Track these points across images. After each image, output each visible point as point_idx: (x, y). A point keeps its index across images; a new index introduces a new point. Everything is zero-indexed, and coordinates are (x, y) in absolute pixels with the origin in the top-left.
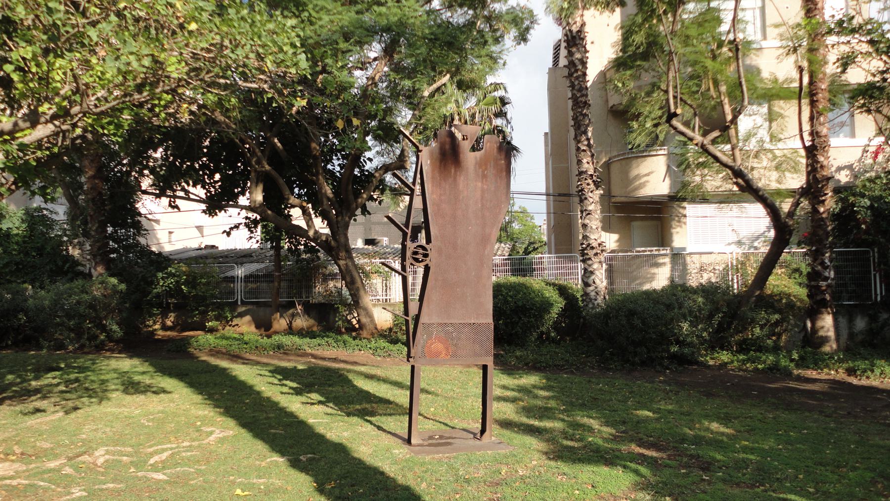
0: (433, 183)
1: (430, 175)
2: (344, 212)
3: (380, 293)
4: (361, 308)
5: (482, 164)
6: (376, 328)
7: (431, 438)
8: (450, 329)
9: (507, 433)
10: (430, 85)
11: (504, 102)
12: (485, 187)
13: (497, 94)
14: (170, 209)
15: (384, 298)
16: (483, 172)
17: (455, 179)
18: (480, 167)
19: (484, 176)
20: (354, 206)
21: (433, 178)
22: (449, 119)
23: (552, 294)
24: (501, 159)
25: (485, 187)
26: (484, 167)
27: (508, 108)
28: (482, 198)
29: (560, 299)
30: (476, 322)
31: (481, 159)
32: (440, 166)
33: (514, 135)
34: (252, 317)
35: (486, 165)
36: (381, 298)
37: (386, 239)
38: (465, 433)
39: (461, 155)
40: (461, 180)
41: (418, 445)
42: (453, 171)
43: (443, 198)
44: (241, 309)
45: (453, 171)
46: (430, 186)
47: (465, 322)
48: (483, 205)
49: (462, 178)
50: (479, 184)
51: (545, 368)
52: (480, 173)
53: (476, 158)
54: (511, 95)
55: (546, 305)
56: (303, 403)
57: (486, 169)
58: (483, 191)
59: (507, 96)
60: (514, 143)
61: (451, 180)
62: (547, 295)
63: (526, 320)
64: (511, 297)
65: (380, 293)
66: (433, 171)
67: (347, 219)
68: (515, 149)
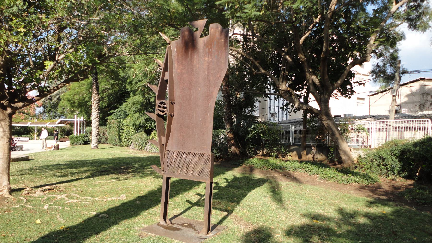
0: (178, 62)
1: (176, 58)
2: (325, 92)
5: (209, 45)
8: (184, 155)
9: (168, 231)
12: (210, 60)
16: (209, 50)
17: (191, 57)
18: (207, 47)
19: (210, 53)
20: (331, 88)
21: (178, 59)
24: (221, 39)
25: (210, 60)
26: (209, 47)
31: (207, 41)
34: (297, 152)
35: (211, 45)
36: (367, 145)
42: (190, 53)
43: (184, 71)
44: (292, 148)
48: (208, 73)
49: (195, 56)
50: (206, 59)
53: (204, 41)
58: (209, 63)
66: (178, 55)
67: (326, 96)
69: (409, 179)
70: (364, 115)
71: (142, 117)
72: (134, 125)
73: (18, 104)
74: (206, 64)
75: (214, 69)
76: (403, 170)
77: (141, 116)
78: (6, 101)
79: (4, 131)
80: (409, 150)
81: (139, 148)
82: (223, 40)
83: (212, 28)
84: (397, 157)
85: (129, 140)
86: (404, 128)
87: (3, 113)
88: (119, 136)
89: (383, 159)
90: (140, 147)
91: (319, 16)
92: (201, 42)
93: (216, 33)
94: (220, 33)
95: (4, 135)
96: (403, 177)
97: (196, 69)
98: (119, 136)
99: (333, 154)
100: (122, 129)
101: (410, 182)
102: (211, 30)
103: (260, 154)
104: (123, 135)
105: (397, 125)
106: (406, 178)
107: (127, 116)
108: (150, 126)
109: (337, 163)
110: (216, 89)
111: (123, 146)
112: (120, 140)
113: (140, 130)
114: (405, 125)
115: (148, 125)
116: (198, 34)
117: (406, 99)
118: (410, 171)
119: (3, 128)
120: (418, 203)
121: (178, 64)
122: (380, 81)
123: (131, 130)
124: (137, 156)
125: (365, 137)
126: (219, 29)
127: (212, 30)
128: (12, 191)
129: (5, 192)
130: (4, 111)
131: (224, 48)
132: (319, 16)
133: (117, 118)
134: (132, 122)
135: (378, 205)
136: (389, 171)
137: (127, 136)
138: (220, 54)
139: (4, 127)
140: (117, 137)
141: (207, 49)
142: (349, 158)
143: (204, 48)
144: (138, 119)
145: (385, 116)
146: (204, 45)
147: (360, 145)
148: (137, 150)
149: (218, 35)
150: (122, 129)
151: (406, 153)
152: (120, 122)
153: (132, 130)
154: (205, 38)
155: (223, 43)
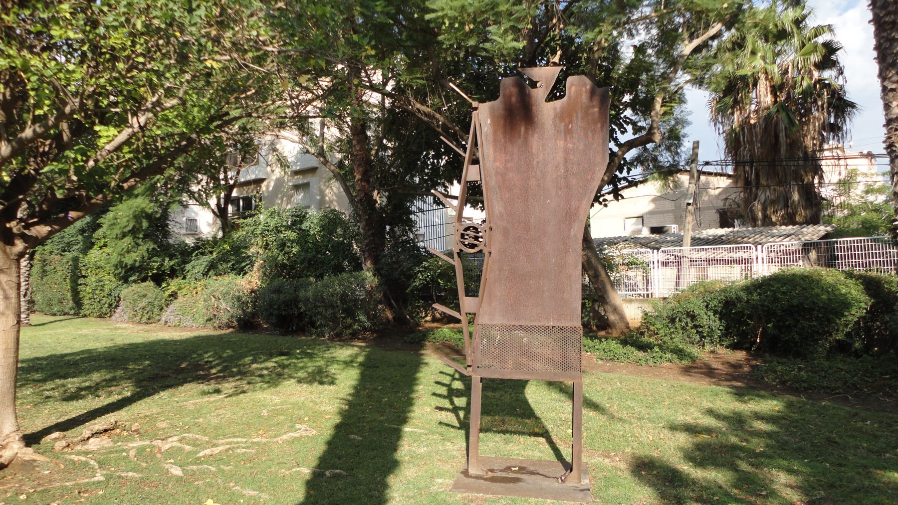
1: (491, 138)
3: (641, 286)
4: (607, 303)
5: (565, 116)
6: (628, 328)
7: (508, 469)
10: (692, 37)
11: (830, 49)
12: (570, 146)
13: (821, 40)
14: (435, 207)
15: (645, 292)
16: (566, 126)
17: (526, 140)
19: (568, 132)
22: (751, 81)
23: (855, 291)
24: (593, 107)
25: (570, 146)
26: (567, 120)
27: (840, 56)
28: (566, 161)
29: (864, 297)
30: (557, 324)
31: (562, 109)
32: (505, 126)
33: (847, 87)
35: (570, 116)
36: (642, 292)
37: (674, 226)
38: (547, 474)
39: (534, 108)
40: (535, 142)
41: (477, 477)
42: (523, 129)
45: (523, 129)
46: (491, 151)
47: (541, 324)
48: (567, 170)
49: (536, 137)
50: (561, 143)
51: (806, 389)
52: (562, 128)
53: (555, 109)
54: (839, 38)
55: (845, 304)
56: (437, 408)
57: (571, 122)
58: (567, 151)
59: (835, 39)
60: (849, 97)
61: (520, 141)
62: (844, 291)
63: (806, 324)
64: (784, 293)
65: (641, 286)
66: (495, 132)
68: (852, 105)
69: (737, 349)
70: (607, 237)
71: (140, 248)
72: (120, 265)
73: (38, 228)
74: (560, 156)
75: (579, 164)
76: (726, 333)
77: (138, 245)
78: (18, 224)
79: (6, 297)
80: (739, 299)
81: (144, 319)
82: (596, 109)
83: (572, 85)
84: (715, 312)
85: (103, 302)
86: (709, 262)
87: (5, 252)
88: (75, 293)
89: (693, 317)
90: (147, 316)
91: (559, 53)
92: (547, 111)
93: (581, 95)
94: (589, 94)
95: (7, 307)
96: (727, 347)
97: (538, 162)
98: (75, 293)
99: (589, 312)
100: (84, 277)
101: (740, 355)
102: (570, 88)
103: (428, 318)
104: (86, 292)
105: (695, 256)
106: (734, 347)
107: (93, 244)
108: (158, 268)
109: (594, 328)
110: (584, 202)
111: (85, 316)
112: (78, 303)
113: (132, 278)
114: (703, 255)
115: (156, 265)
116: (540, 94)
117: (651, 206)
118: (743, 335)
119: (4, 291)
120: (797, 388)
121: (495, 151)
122: (654, 178)
123: (107, 277)
124: (152, 339)
125: (639, 278)
126: (588, 87)
127: (573, 89)
128: (31, 440)
129: (15, 449)
130: (8, 248)
131: (599, 125)
132: (559, 53)
133: (64, 251)
134: (114, 259)
135: (762, 393)
136: (704, 337)
137: (97, 292)
138: (590, 133)
139: (6, 287)
140: (69, 295)
141: (563, 124)
142: (622, 317)
143: (554, 121)
144: (128, 252)
145: (620, 237)
146: (556, 116)
147: (629, 293)
148: (139, 323)
149: (585, 98)
150: (84, 277)
151: (734, 304)
152: (76, 260)
153: (110, 281)
154: (558, 103)
155: (597, 115)
